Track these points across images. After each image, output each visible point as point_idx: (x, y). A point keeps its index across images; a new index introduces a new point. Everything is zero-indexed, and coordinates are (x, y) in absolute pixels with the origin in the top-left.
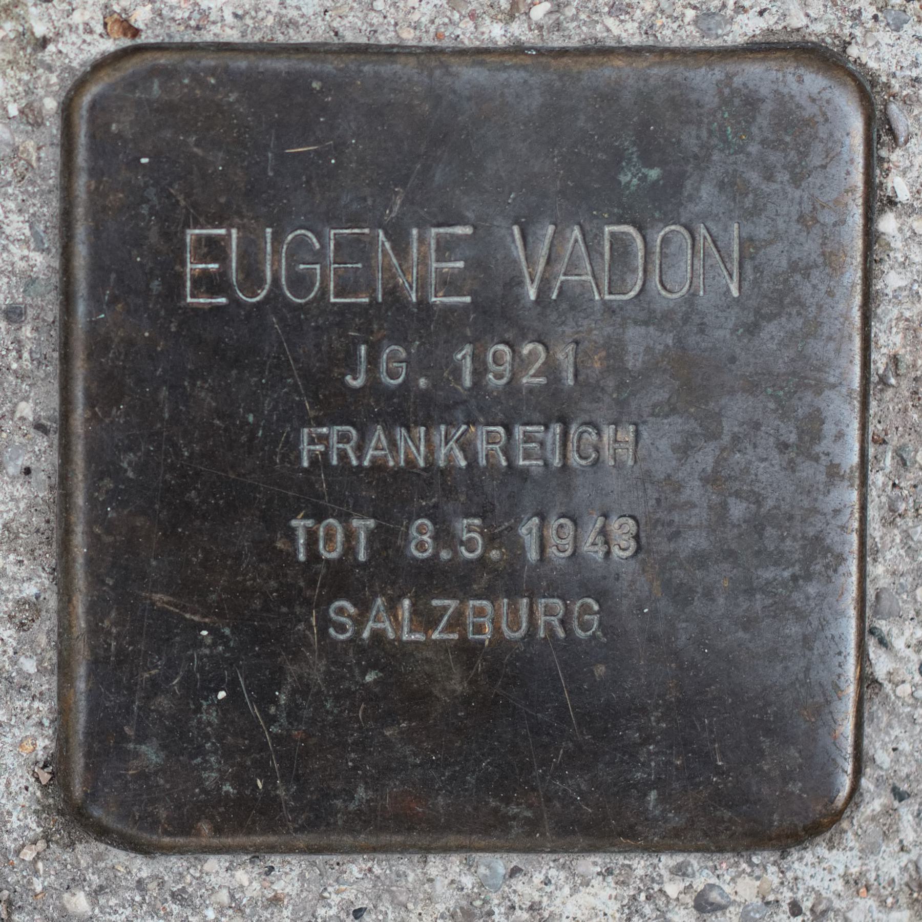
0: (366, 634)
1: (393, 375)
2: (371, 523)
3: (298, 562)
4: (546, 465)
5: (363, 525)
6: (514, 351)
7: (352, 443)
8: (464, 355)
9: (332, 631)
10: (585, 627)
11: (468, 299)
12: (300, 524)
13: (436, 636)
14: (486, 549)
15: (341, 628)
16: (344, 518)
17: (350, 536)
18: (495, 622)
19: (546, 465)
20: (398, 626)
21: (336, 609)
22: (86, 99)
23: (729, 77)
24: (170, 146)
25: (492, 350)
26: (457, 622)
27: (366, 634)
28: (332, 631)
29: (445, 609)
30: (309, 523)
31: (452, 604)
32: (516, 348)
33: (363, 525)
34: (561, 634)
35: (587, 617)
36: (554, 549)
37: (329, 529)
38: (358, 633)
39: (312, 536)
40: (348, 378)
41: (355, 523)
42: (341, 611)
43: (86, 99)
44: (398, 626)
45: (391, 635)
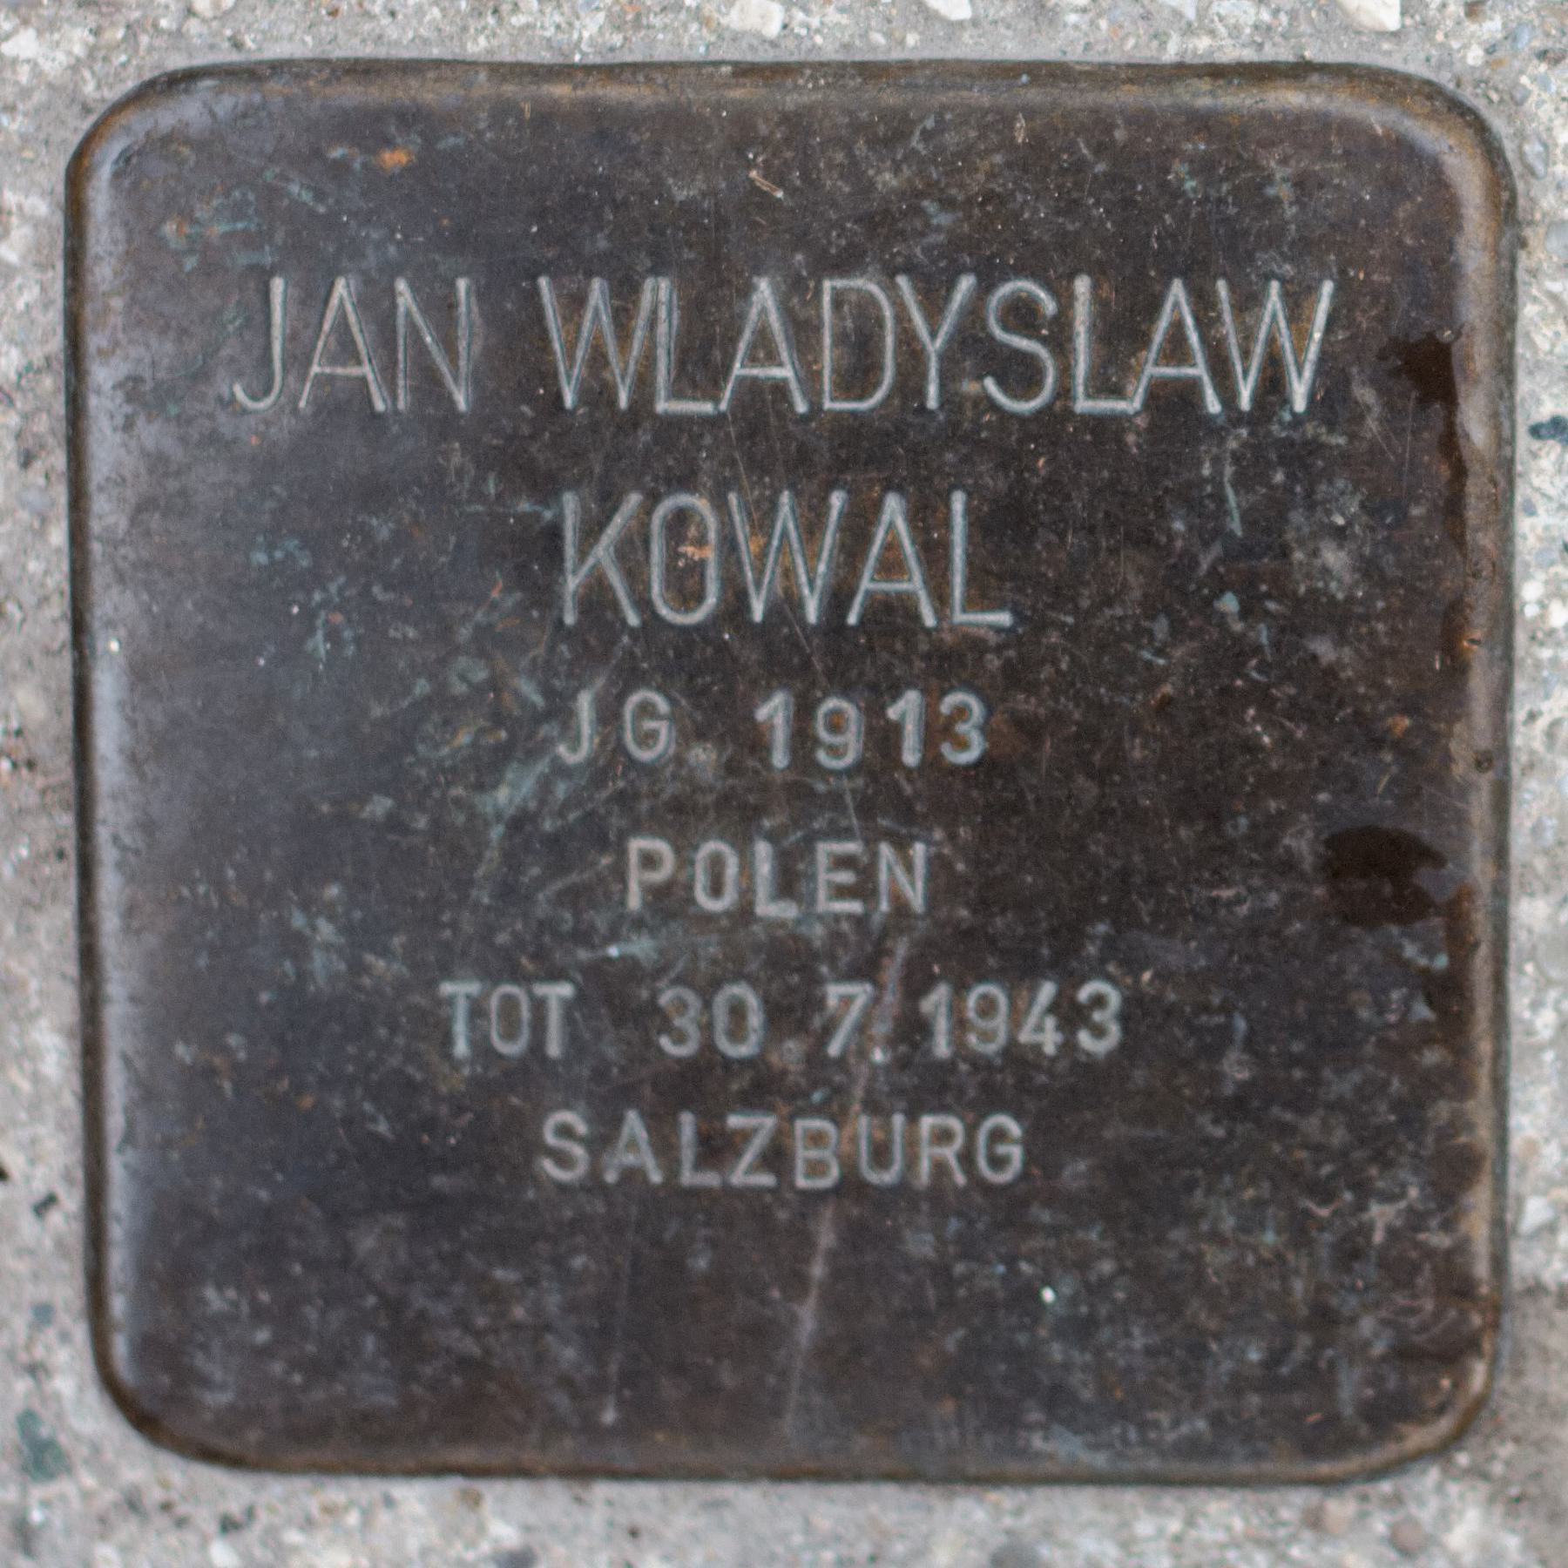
10: (998, 1163)
15: (563, 1160)
26: (777, 1157)
27: (611, 1177)
29: (752, 1169)
34: (960, 1179)
41: (541, 989)
42: (565, 1131)
45: (656, 1177)
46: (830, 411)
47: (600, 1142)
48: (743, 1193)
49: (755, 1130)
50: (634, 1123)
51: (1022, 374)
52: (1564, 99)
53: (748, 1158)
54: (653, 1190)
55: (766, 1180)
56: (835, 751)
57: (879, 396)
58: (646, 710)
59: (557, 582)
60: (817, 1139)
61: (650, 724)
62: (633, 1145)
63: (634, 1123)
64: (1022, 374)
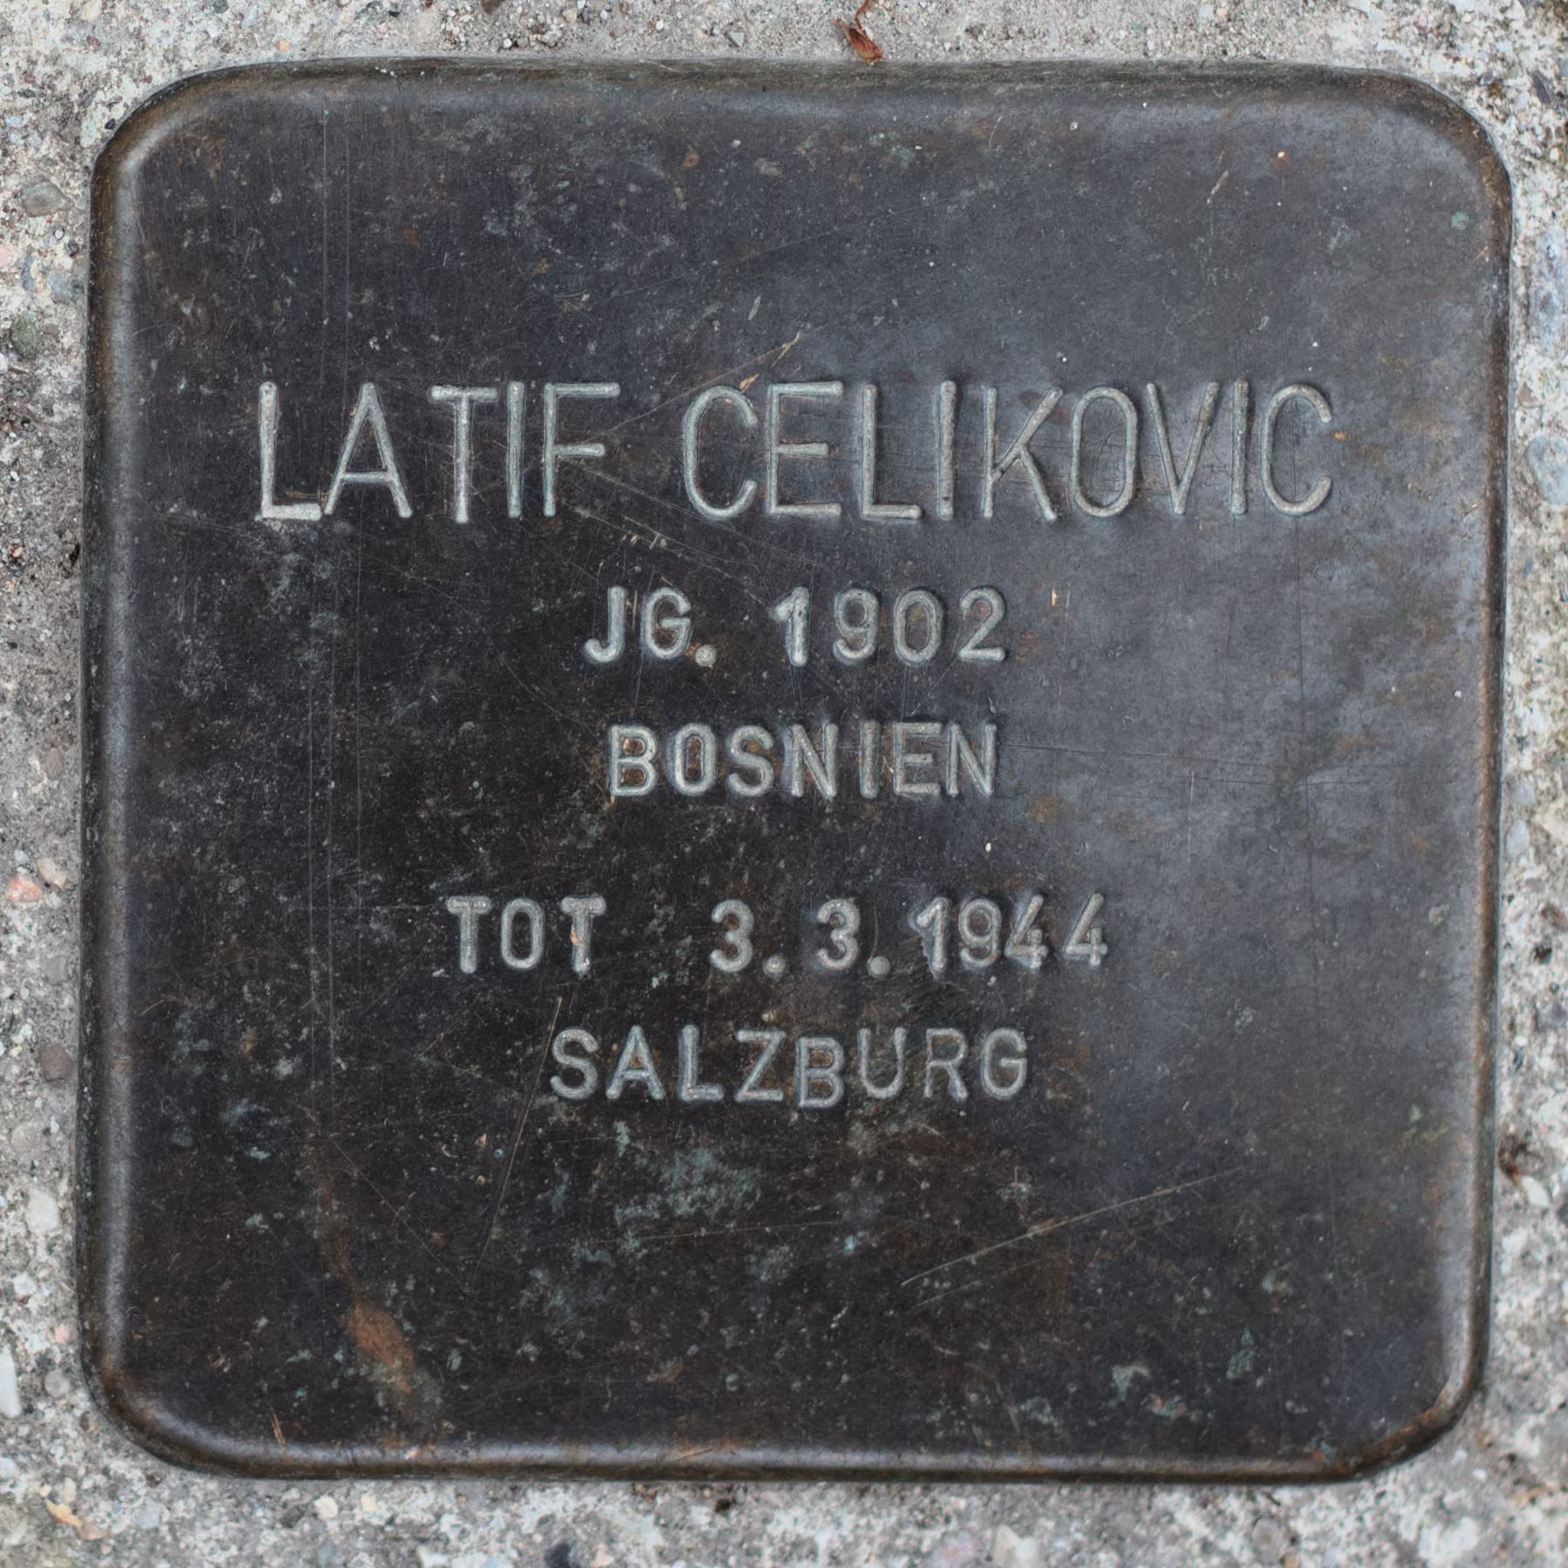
0: (613, 1092)
2: (598, 905)
4: (943, 791)
5: (583, 909)
6: (945, 607)
7: (649, 755)
8: (792, 609)
10: (1004, 1078)
12: (467, 908)
13: (743, 1094)
15: (573, 1077)
16: (548, 899)
17: (559, 928)
19: (943, 791)
22: (133, 161)
23: (1468, 1131)
24: (242, 225)
30: (483, 904)
32: (951, 602)
33: (583, 909)
34: (960, 1093)
35: (1004, 1062)
37: (521, 920)
41: (568, 904)
42: (574, 1048)
43: (133, 161)
45: (657, 1093)
50: (636, 1043)
55: (777, 1095)
56: (978, 953)
60: (818, 1060)
61: (668, 623)
62: (636, 1064)
63: (636, 1043)
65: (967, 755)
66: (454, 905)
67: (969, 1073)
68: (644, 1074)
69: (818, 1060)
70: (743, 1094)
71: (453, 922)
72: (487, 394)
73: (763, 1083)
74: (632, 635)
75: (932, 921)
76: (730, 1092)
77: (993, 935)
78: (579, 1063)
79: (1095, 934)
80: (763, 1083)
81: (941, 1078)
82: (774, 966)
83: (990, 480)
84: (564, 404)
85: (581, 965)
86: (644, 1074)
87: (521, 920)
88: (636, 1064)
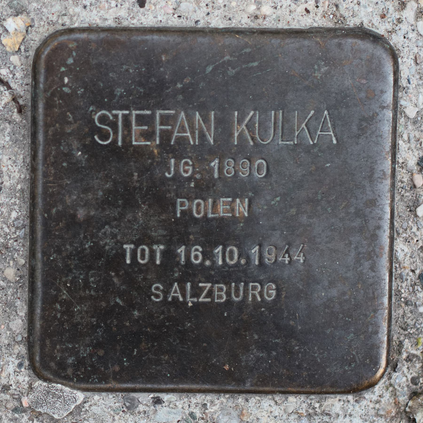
1: (186, 171)
2: (162, 247)
3: (156, 265)
8: (215, 164)
9: (153, 297)
10: (269, 296)
11: (172, 143)
13: (200, 300)
14: (204, 260)
15: (157, 296)
16: (149, 245)
17: (152, 253)
18: (228, 294)
20: (184, 296)
21: (154, 287)
25: (227, 161)
26: (210, 294)
27: (170, 299)
28: (153, 297)
29: (205, 287)
30: (132, 246)
31: (209, 285)
33: (159, 248)
34: (259, 299)
36: (267, 260)
38: (165, 298)
39: (134, 253)
40: (167, 174)
41: (155, 247)
42: (157, 288)
44: (184, 296)
45: (181, 299)
46: (217, 303)
47: (166, 292)
48: (203, 303)
49: (204, 298)
51: (104, 136)
52: (421, 12)
53: (204, 294)
54: (181, 302)
55: (209, 300)
57: (111, 136)
58: (186, 164)
59: (209, 115)
61: (187, 168)
64: (104, 136)
65: (241, 206)
66: (125, 246)
67: (261, 294)
68: (178, 295)
69: (221, 289)
70: (200, 300)
71: (125, 251)
72: (127, 112)
73: (206, 297)
74: (177, 171)
75: (181, 251)
76: (198, 299)
77: (273, 255)
78: (158, 292)
79: (302, 254)
80: (206, 297)
81: (254, 296)
82: (208, 263)
83: (236, 135)
84: (137, 115)
85: (158, 262)
86: (178, 295)
87: (143, 251)
88: (176, 292)
